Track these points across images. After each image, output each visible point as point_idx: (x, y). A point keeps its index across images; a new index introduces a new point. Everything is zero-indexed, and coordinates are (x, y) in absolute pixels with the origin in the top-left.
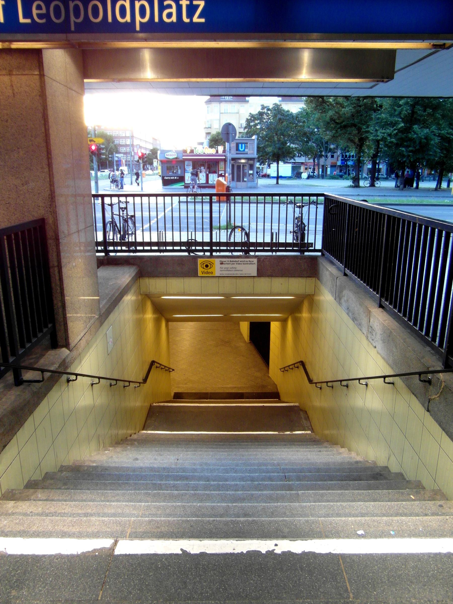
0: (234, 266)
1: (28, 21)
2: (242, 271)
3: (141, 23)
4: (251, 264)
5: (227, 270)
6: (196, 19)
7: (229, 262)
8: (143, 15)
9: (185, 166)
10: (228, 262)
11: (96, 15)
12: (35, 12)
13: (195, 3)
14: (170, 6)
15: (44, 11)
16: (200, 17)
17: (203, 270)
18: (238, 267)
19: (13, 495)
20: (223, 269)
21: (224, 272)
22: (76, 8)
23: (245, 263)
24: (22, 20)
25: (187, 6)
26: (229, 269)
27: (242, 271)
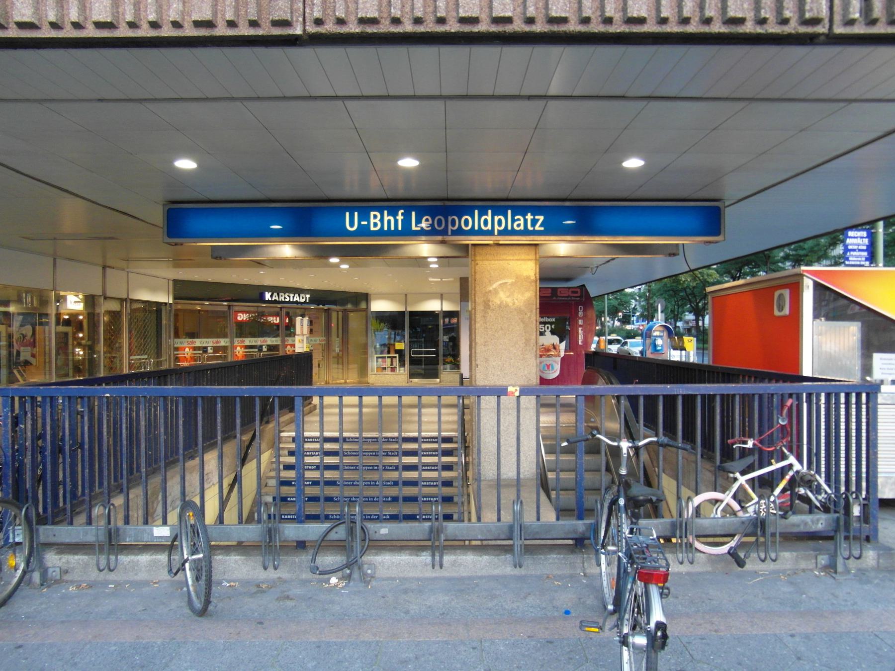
6: (537, 228)
13: (537, 217)
14: (519, 220)
16: (541, 226)
24: (414, 228)
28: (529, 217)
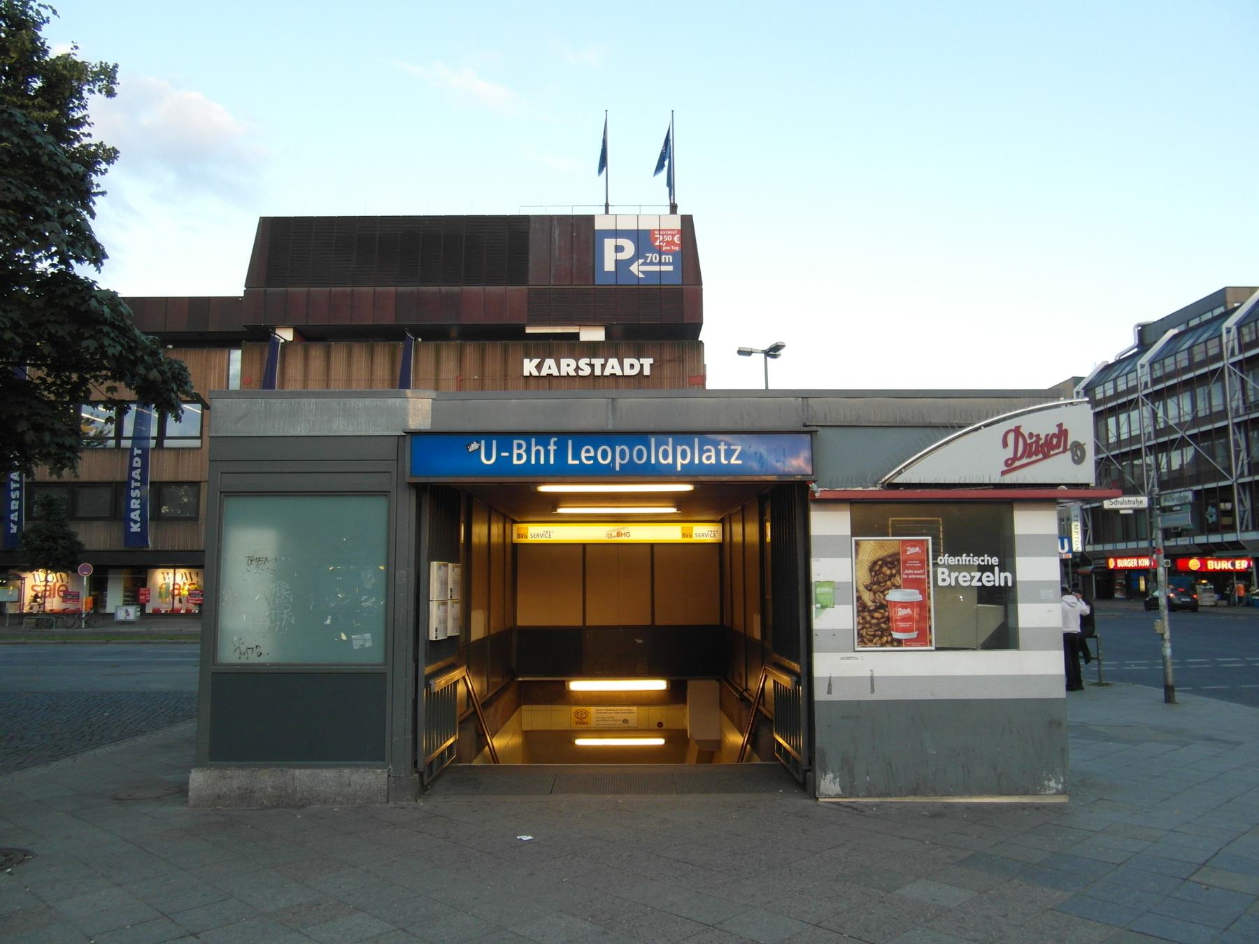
6: (733, 461)
8: (622, 458)
9: (61, 480)
11: (640, 457)
12: (583, 455)
15: (592, 454)
19: (141, 425)
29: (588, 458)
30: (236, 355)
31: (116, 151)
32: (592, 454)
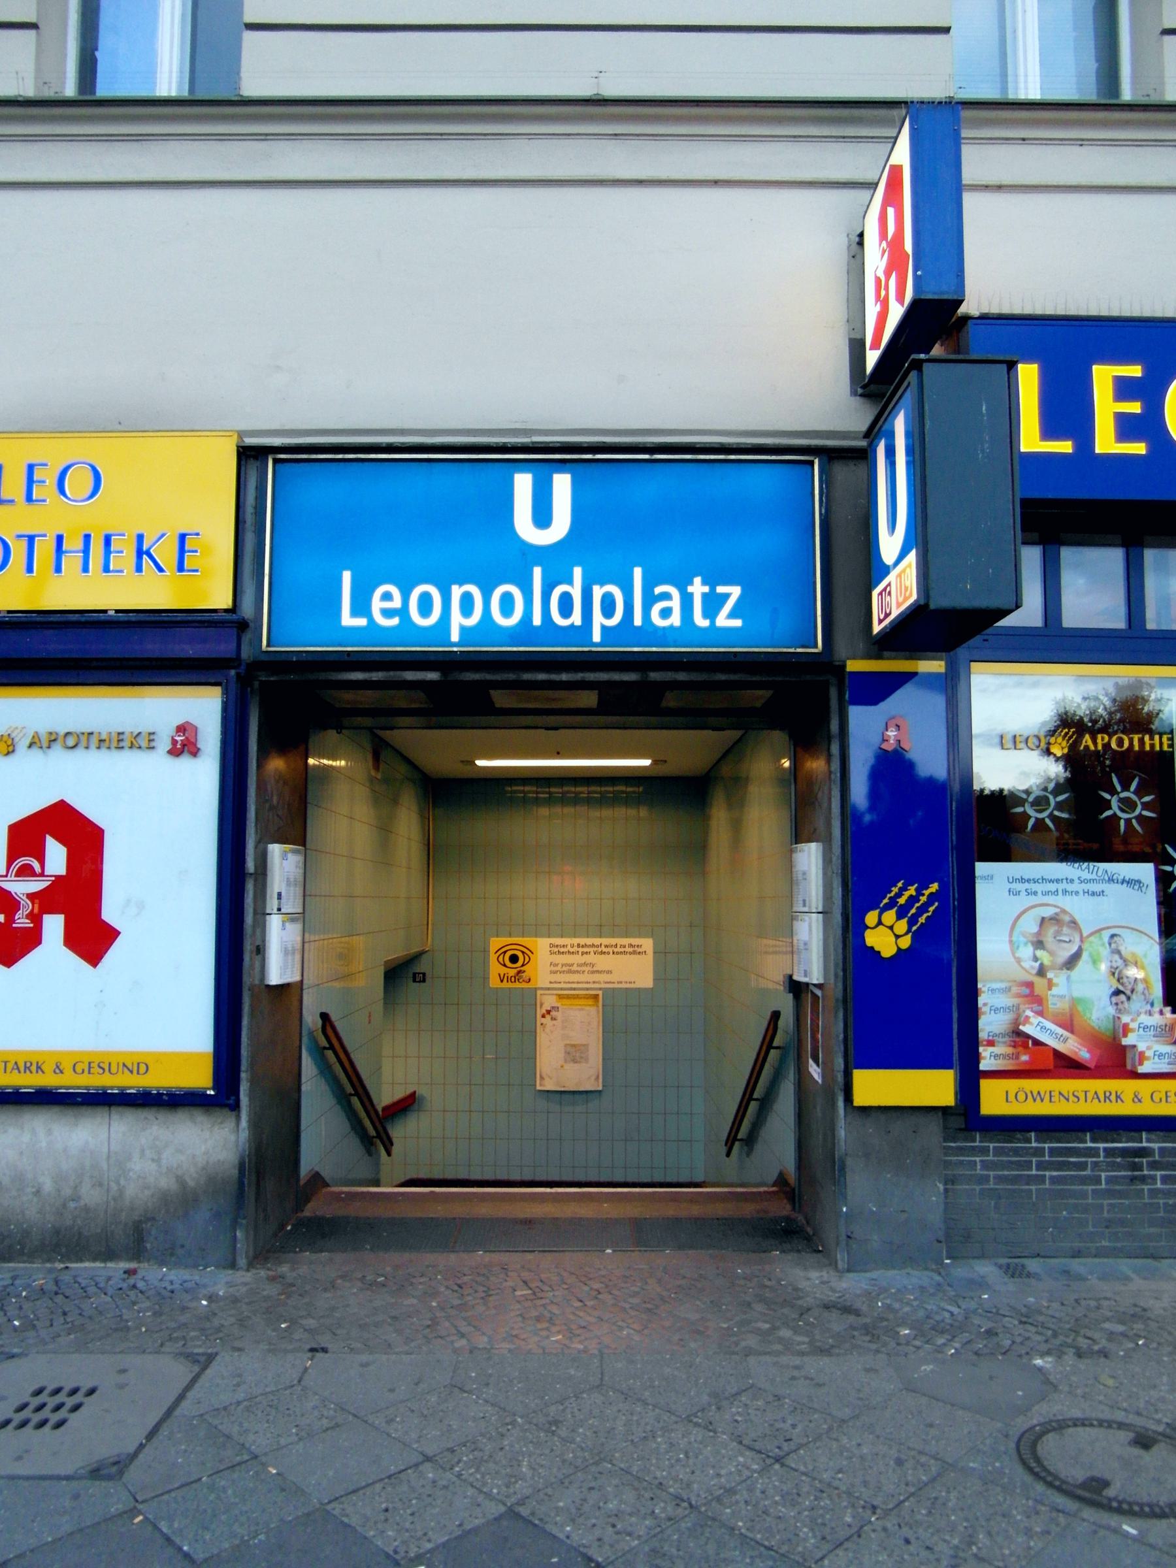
0: (586, 959)
1: (362, 622)
2: (609, 972)
3: (603, 628)
4: (634, 953)
5: (570, 972)
6: (722, 621)
7: (575, 949)
10: (572, 946)
12: (377, 604)
13: (721, 589)
14: (666, 596)
15: (397, 603)
17: (503, 970)
18: (602, 962)
20: (559, 968)
21: (558, 977)
22: (467, 600)
23: (618, 949)
25: (705, 596)
26: (575, 968)
27: (609, 972)
28: (698, 588)
29: (387, 613)
30: (311, 761)
31: (181, 729)
32: (397, 603)
